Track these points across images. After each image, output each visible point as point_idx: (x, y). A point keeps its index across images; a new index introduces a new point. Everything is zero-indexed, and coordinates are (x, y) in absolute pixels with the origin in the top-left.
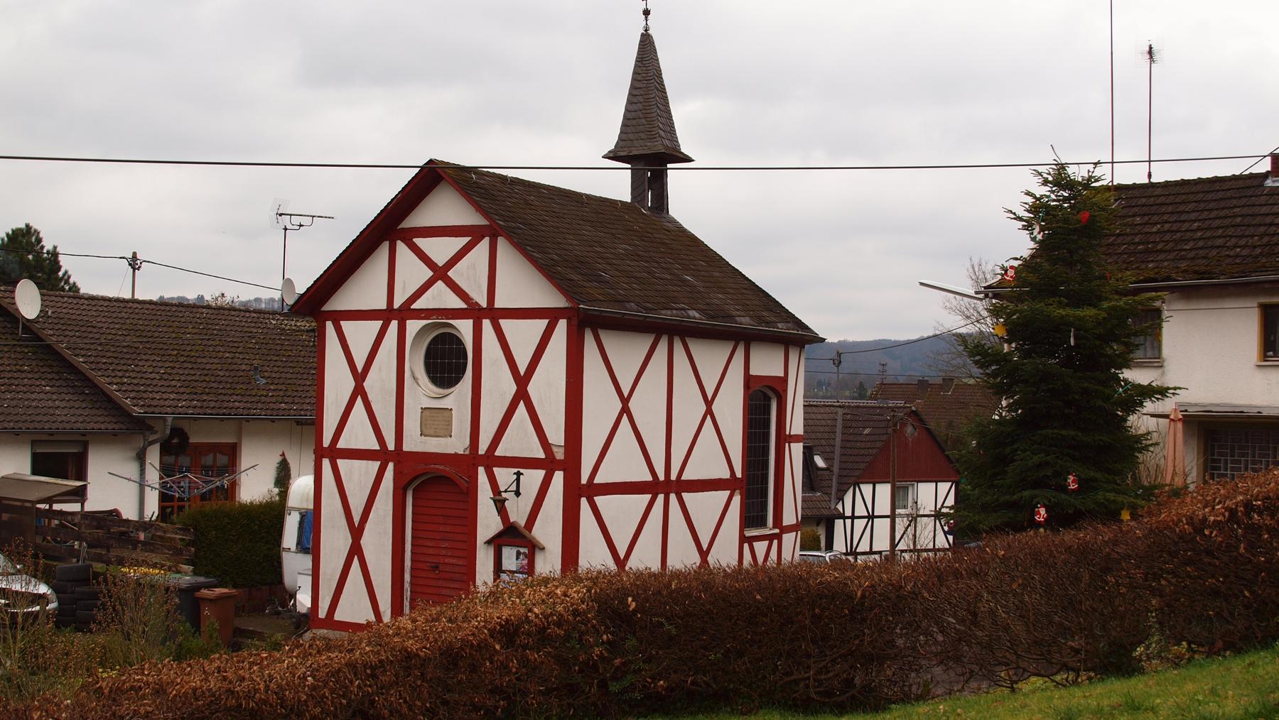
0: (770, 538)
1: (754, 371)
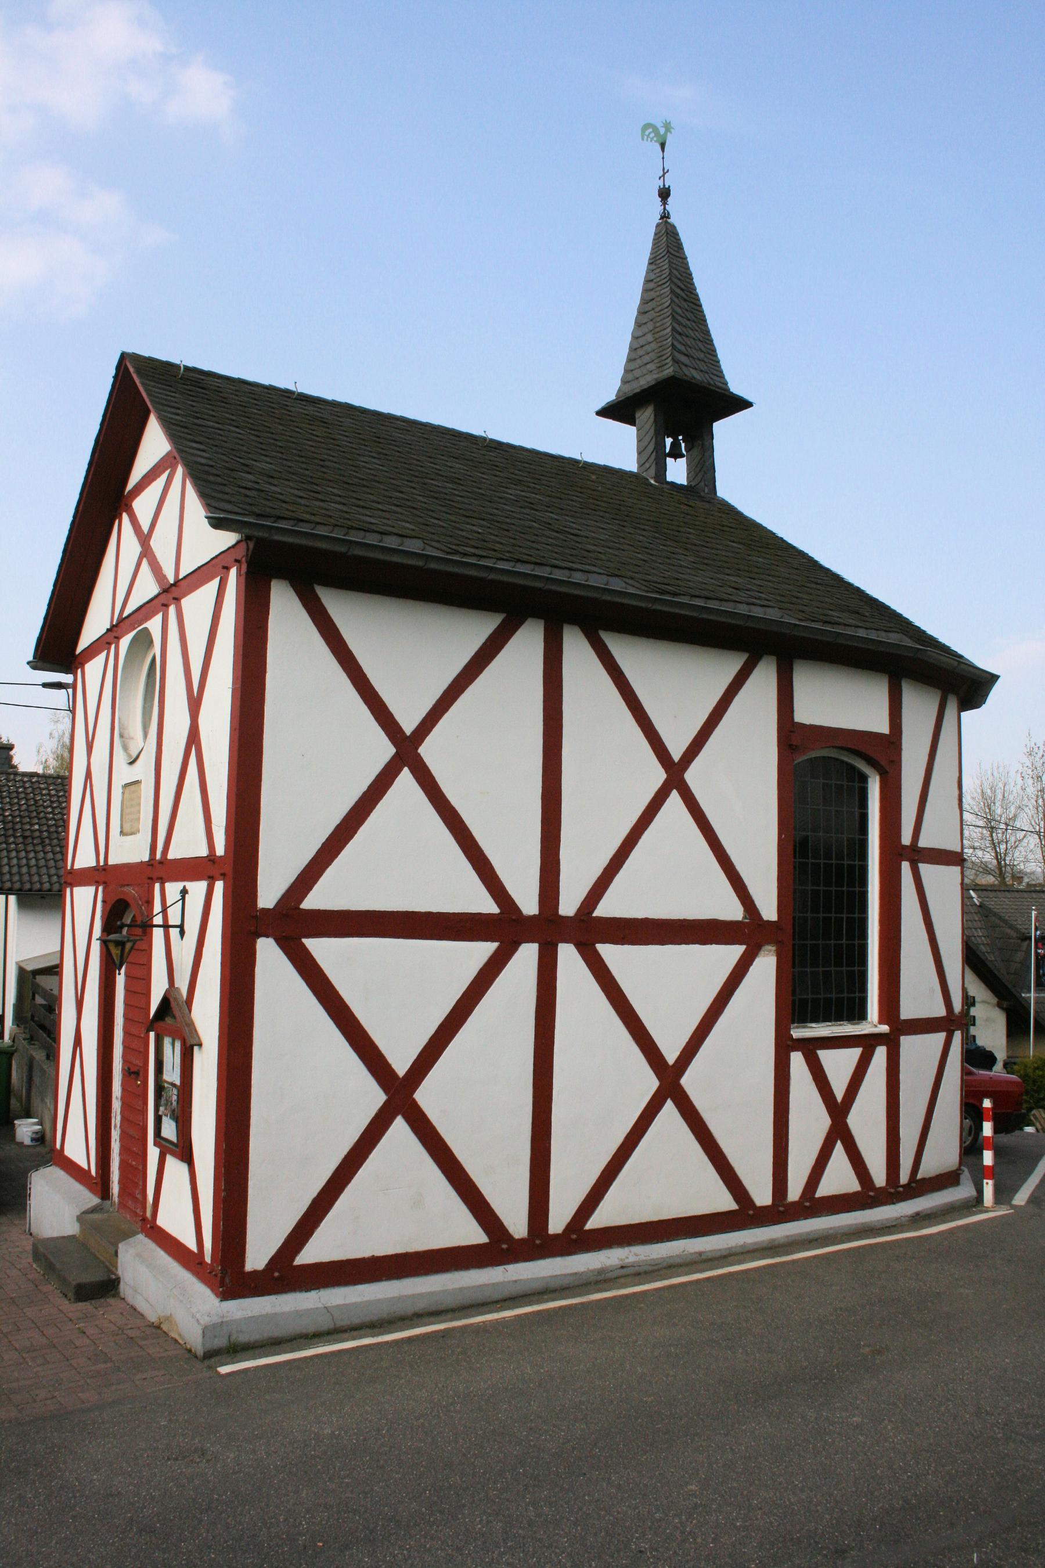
0: (868, 1043)
1: (805, 713)
